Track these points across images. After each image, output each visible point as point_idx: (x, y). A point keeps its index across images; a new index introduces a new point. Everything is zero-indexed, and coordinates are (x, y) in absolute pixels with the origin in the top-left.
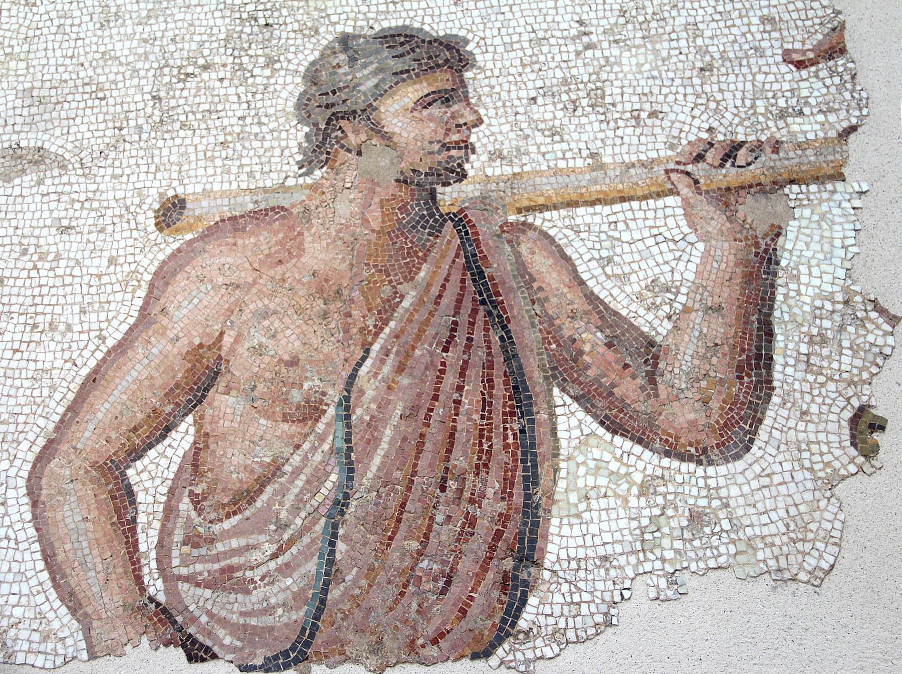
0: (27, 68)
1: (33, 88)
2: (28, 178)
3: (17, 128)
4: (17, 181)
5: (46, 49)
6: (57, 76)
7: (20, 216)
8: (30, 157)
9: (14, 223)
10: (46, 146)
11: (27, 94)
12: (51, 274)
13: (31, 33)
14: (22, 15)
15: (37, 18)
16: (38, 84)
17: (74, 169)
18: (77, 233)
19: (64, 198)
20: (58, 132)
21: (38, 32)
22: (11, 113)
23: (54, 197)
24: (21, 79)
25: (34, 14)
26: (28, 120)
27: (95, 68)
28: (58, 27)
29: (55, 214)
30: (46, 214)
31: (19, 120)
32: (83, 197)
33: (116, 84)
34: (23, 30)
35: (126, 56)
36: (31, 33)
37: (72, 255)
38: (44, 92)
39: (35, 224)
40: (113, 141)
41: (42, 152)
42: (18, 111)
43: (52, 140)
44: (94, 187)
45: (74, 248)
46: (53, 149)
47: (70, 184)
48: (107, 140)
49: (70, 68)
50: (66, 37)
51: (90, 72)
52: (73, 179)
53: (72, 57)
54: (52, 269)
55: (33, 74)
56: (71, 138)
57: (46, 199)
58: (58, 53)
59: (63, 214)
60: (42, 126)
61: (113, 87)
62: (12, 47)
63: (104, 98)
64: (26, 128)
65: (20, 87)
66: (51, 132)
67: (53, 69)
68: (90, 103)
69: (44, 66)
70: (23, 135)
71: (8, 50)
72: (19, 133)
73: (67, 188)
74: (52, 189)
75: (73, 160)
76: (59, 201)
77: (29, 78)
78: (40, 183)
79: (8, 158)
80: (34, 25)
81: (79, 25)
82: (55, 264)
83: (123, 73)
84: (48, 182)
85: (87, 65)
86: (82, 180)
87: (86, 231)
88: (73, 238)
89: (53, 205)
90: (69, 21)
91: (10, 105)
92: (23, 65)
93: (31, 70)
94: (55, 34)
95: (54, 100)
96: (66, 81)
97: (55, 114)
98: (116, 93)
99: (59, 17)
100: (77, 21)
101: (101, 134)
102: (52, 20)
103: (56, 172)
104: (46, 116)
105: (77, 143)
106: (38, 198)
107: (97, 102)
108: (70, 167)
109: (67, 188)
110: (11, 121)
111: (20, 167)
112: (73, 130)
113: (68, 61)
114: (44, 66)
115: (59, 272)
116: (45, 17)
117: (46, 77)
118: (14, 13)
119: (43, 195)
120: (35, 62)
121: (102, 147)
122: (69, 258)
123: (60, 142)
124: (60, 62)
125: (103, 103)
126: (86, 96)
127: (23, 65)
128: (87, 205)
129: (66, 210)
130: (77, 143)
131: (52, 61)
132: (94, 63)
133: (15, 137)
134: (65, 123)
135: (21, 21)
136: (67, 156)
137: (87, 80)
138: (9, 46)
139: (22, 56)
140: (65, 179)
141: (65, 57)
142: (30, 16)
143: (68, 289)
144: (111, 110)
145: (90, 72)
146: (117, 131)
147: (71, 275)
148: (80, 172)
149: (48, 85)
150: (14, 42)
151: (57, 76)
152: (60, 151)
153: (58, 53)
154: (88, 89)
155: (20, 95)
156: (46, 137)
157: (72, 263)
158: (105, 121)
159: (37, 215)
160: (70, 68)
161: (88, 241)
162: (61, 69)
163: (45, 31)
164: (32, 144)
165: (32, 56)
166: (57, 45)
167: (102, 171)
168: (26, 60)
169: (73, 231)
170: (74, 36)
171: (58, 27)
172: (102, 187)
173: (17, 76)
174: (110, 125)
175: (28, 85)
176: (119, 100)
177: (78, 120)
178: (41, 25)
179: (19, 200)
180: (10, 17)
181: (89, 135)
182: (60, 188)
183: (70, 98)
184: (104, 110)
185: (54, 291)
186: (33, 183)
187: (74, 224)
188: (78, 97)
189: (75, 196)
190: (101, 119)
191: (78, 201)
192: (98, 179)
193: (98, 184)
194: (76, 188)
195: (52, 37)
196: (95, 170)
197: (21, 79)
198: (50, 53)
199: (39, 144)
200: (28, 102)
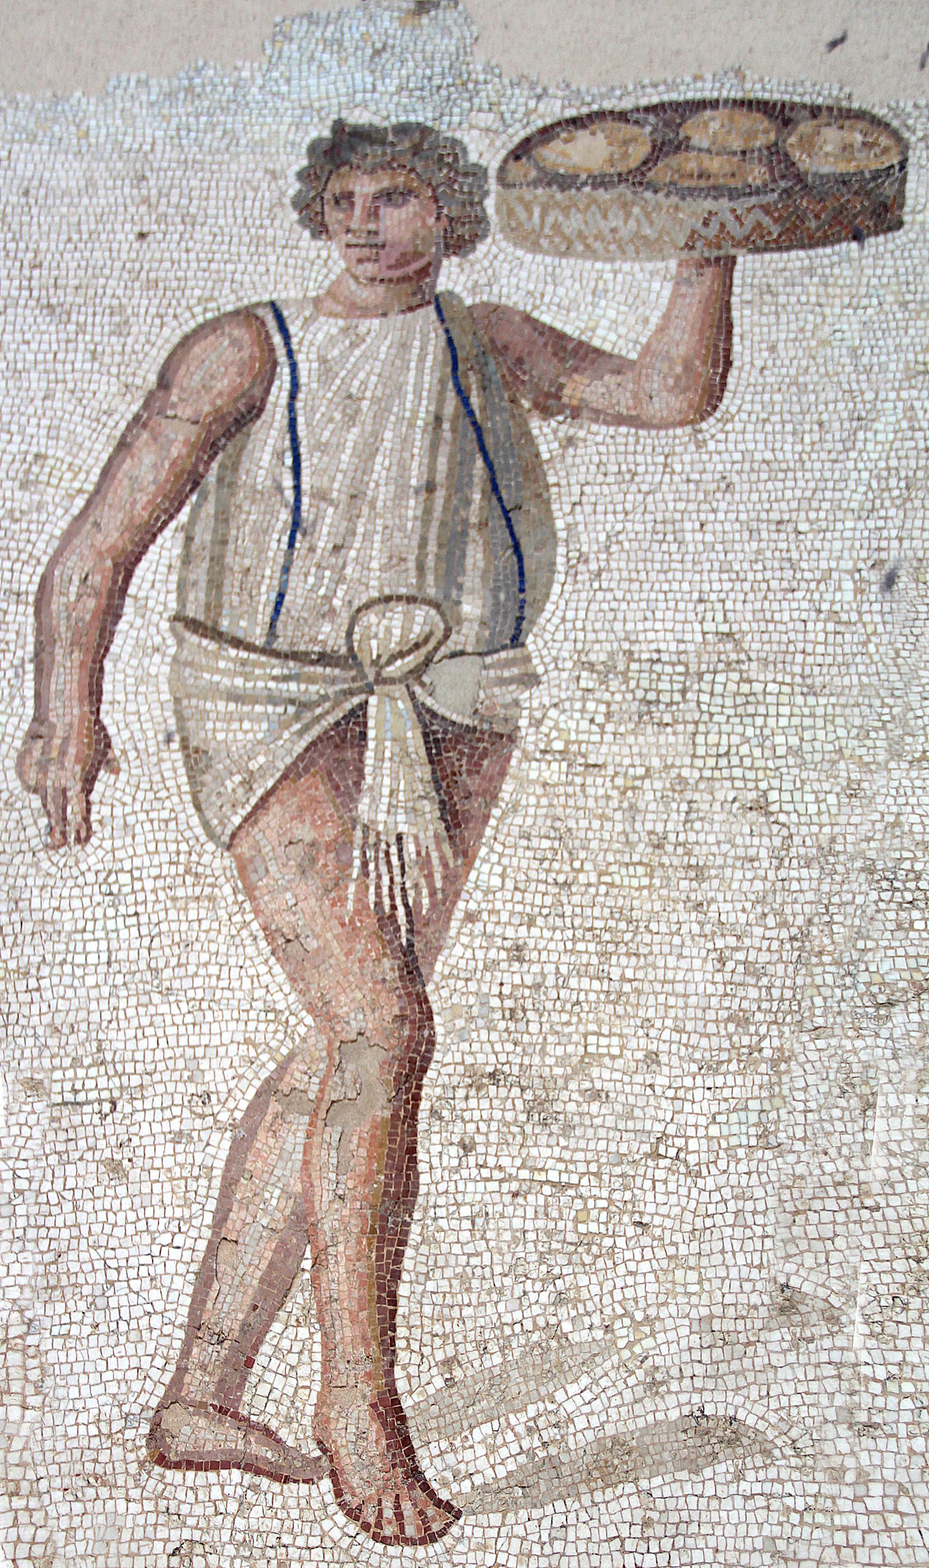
0: (700, 1282)
1: (712, 1317)
2: (721, 1468)
3: (698, 1383)
4: (708, 1472)
5: (723, 1252)
6: (743, 1298)
7: (718, 1530)
8: (719, 1433)
9: (712, 1542)
10: (741, 1415)
11: (705, 1326)
12: (859, 1507)
13: (699, 1224)
14: (683, 1191)
15: (705, 1197)
16: (717, 1310)
17: (784, 1457)
18: (888, 1436)
19: (775, 1504)
20: (809, 1260)
21: (709, 1222)
22: (686, 1357)
23: (761, 1502)
24: (694, 1300)
25: (701, 1190)
26: (711, 1370)
27: (848, 1159)
28: (736, 1213)
29: (766, 1530)
30: (754, 1531)
31: (699, 1369)
32: (881, 1373)
33: (892, 1186)
34: (688, 1217)
35: (899, 1142)
36: (699, 1224)
37: (889, 1474)
38: (728, 1325)
39: (739, 1544)
40: (911, 1280)
41: (735, 1425)
42: (696, 1355)
43: (803, 1272)
44: (898, 1357)
45: (889, 1463)
46: (751, 1421)
47: (781, 1482)
48: (900, 1278)
49: (759, 1286)
50: (749, 1233)
51: (842, 1165)
52: (784, 1475)
53: (760, 1267)
54: (856, 1499)
55: (710, 1292)
56: (774, 1405)
57: (750, 1504)
58: (741, 1259)
59: (777, 1530)
60: (730, 1380)
61: (888, 1190)
62: (675, 1244)
63: (878, 1208)
64: (710, 1384)
65: (694, 1314)
66: (745, 1392)
67: (736, 1285)
68: (853, 1214)
69: (723, 1280)
70: (707, 1396)
71: (671, 1250)
72: (701, 1391)
73: (777, 1488)
74: (757, 1488)
75: (779, 1442)
76: (839, 1377)
77: (705, 1299)
78: (739, 1476)
79: (691, 1433)
80: (701, 1210)
81: (764, 1213)
82: (861, 1491)
83: (900, 1170)
84: (750, 1475)
85: (833, 1152)
86: (796, 1475)
87: (903, 1432)
88: (881, 1444)
89: (762, 1515)
90: (749, 1206)
91: (684, 1343)
92: (693, 1276)
93: (706, 1286)
94: (733, 1226)
95: (742, 1338)
96: (756, 1307)
97: (747, 1363)
98: (894, 1201)
99: (736, 1198)
100: (761, 1207)
101: (886, 1266)
102: (725, 1202)
103: (759, 1460)
104: (735, 1366)
105: (783, 1414)
106: (739, 1501)
107: (866, 1214)
108: (777, 1452)
109: (777, 1488)
110: (688, 1372)
111: (708, 1449)
112: (835, 1258)
113: (755, 1274)
114: (723, 1280)
115: (874, 1504)
116: (716, 1197)
117: (729, 1299)
118: (672, 1187)
119: (746, 1498)
120: (710, 1273)
121: (893, 1289)
122: (884, 1481)
123: (760, 1410)
124: (744, 1275)
125: (877, 1215)
126: (844, 1204)
127: (693, 1276)
128: (892, 1387)
129: (780, 1524)
130: (783, 1414)
131: (734, 1273)
132: (845, 1151)
133: (696, 1398)
134: (818, 1245)
135: (684, 1201)
136: (834, 1300)
137: (839, 1178)
138: (673, 1244)
139: (692, 1261)
140: (772, 1473)
141: (750, 1265)
142: (694, 1193)
143: (899, 1538)
144: (895, 1228)
145: (842, 1165)
146: (913, 1264)
147: (896, 1511)
148: (794, 1461)
149: (731, 1312)
150: (677, 1237)
151: (743, 1298)
152: (761, 1425)
153: (741, 1259)
154: (843, 1191)
155: (696, 1327)
156: (739, 1400)
157: (893, 1490)
158: (887, 1246)
159: (742, 1529)
160: (759, 1286)
161: (912, 1452)
162: (747, 1286)
163: (718, 1220)
164: (721, 1412)
165: (704, 1262)
166: (737, 1247)
167: (904, 1331)
168: (697, 1268)
169: (879, 1432)
170: (759, 1231)
171: (736, 1213)
172: (912, 1357)
173: (689, 1294)
174: (899, 1252)
175: (704, 1312)
176: (904, 1213)
177: (840, 1242)
178: (711, 1209)
179: (714, 1503)
180: (668, 1193)
181: (796, 1400)
182: (767, 1488)
183: (817, 1205)
184: (882, 1227)
185: (871, 1539)
186: (785, 1345)
187: (877, 1419)
188: (831, 1204)
189: (789, 1501)
190: (880, 1243)
191: (875, 1380)
192: (902, 1344)
193: (903, 1352)
194: (789, 1488)
195: (728, 1231)
196: (891, 1328)
197: (694, 1300)
198: (729, 1259)
199: (731, 1412)
200: (708, 1340)
